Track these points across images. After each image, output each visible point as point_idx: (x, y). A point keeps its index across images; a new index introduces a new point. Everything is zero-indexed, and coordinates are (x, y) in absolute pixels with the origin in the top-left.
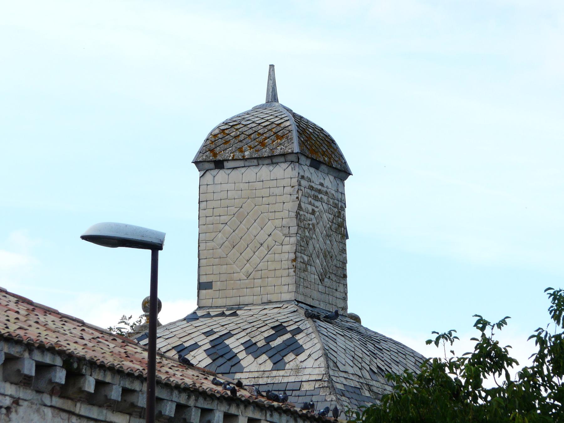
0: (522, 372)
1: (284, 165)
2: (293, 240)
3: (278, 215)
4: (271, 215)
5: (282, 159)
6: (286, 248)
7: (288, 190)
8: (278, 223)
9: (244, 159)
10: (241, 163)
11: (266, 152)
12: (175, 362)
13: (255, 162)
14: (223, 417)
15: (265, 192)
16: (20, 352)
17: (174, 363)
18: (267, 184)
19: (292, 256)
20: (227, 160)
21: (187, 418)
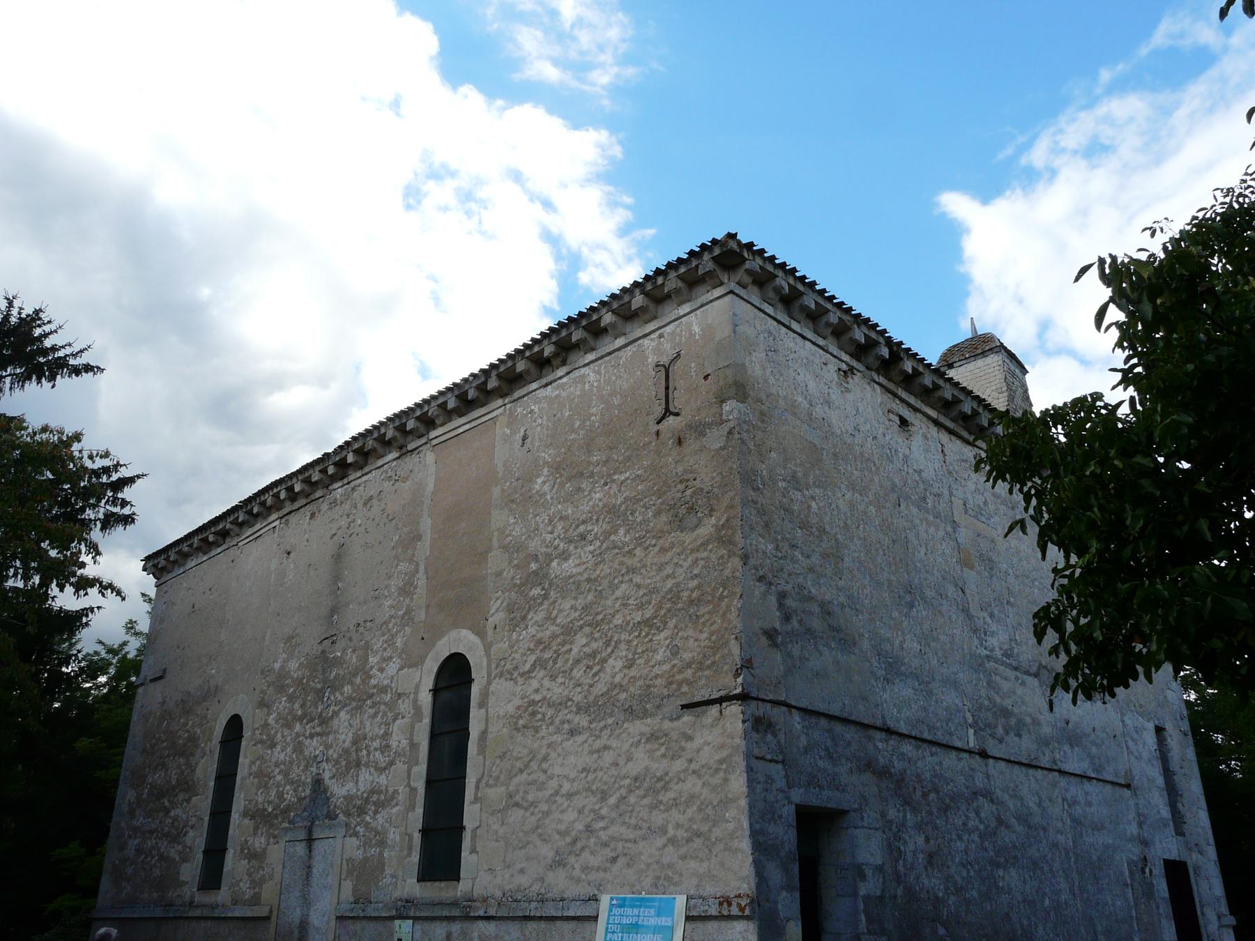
0: (34, 377)
1: (992, 356)
2: (1006, 394)
3: (992, 384)
4: (988, 385)
5: (990, 352)
6: (1001, 400)
7: (997, 368)
8: (994, 388)
9: (966, 359)
10: (964, 362)
11: (979, 351)
12: (206, 913)
13: (973, 359)
14: (1200, 783)
15: (981, 374)
16: (841, 785)
17: (214, 907)
18: (982, 369)
19: (1007, 403)
20: (956, 362)
21: (1189, 863)
